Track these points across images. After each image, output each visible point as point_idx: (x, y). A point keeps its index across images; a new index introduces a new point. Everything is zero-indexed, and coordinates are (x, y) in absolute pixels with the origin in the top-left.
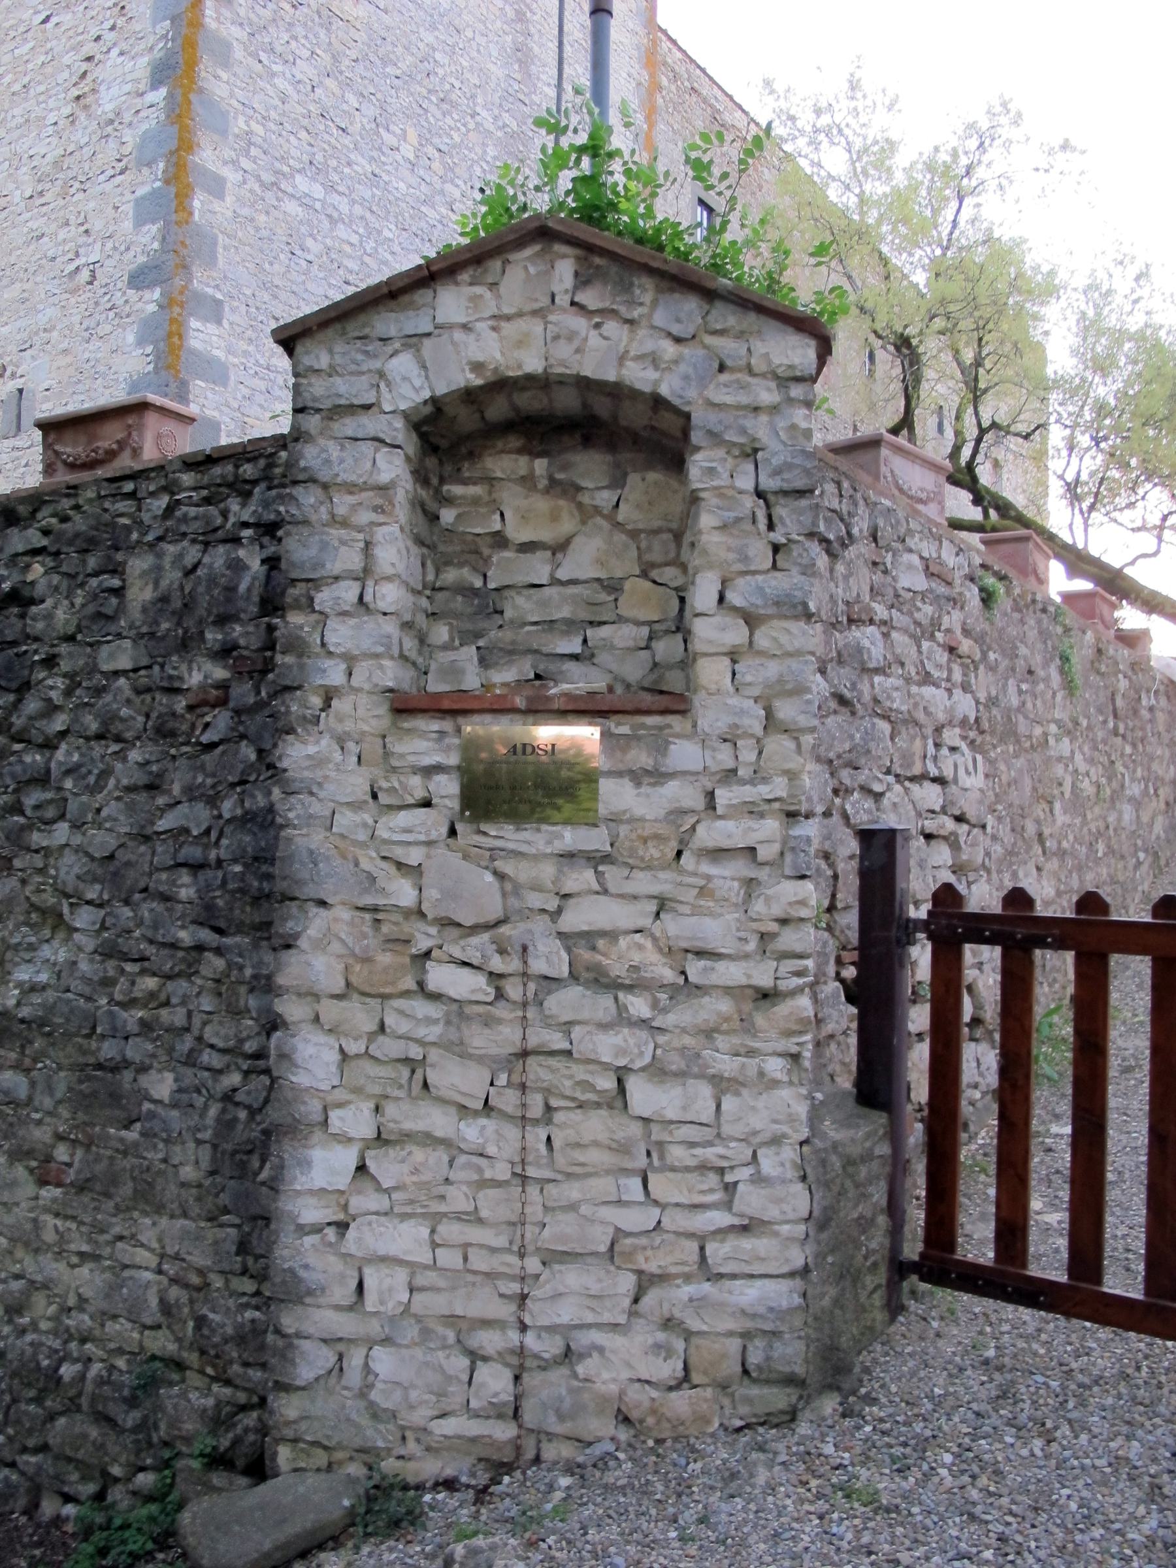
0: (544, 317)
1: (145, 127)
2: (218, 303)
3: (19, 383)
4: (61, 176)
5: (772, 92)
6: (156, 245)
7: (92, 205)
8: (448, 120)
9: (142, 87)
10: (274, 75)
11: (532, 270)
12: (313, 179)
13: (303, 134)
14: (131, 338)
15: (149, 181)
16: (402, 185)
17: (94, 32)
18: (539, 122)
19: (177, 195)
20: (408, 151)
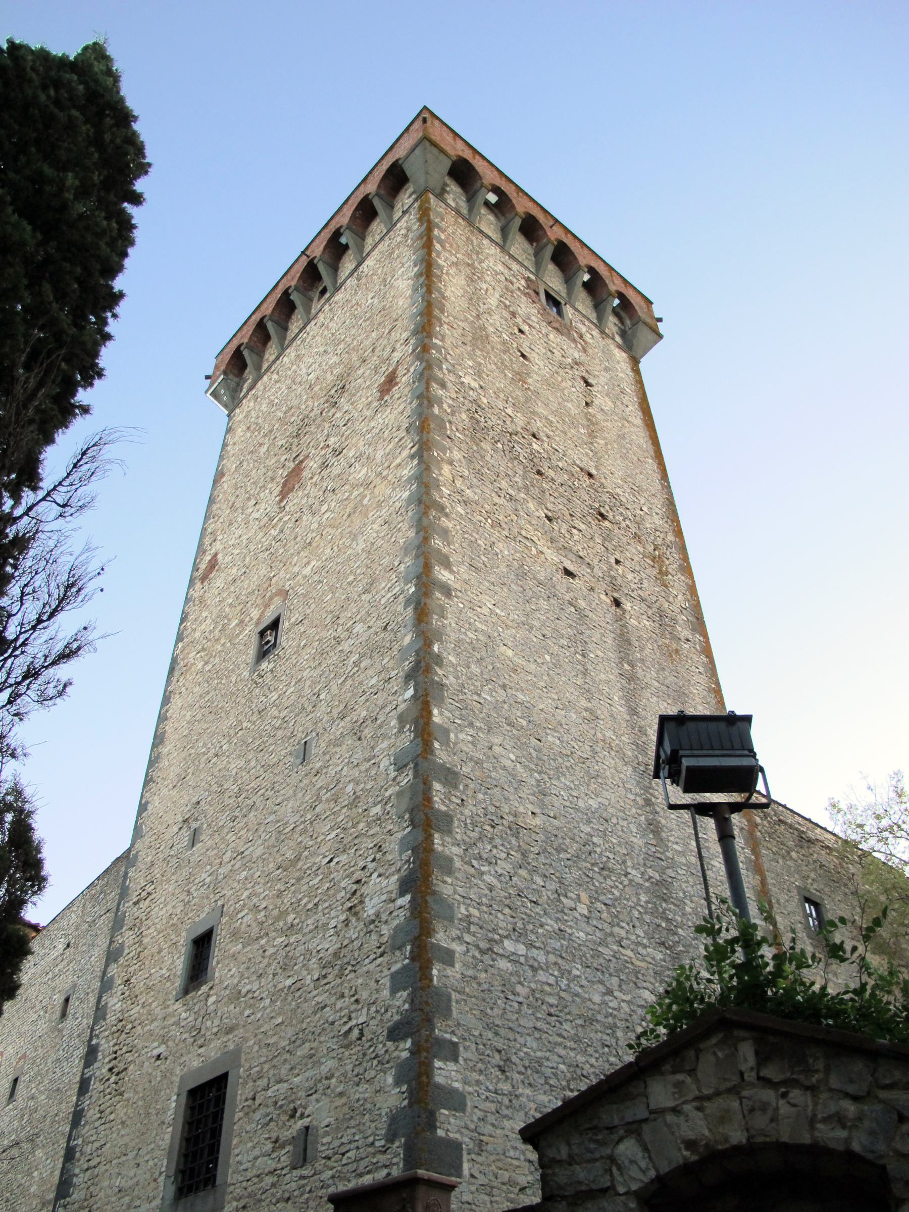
0: (738, 1093)
1: (396, 922)
2: (455, 1045)
3: (306, 1121)
4: (339, 962)
5: (839, 811)
6: (407, 1006)
7: (360, 981)
8: (609, 882)
9: (394, 896)
10: (482, 873)
11: (720, 1054)
12: (517, 941)
13: (507, 911)
14: (390, 1080)
15: (400, 961)
16: (582, 934)
17: (361, 864)
18: (699, 930)
19: (421, 968)
20: (583, 909)
